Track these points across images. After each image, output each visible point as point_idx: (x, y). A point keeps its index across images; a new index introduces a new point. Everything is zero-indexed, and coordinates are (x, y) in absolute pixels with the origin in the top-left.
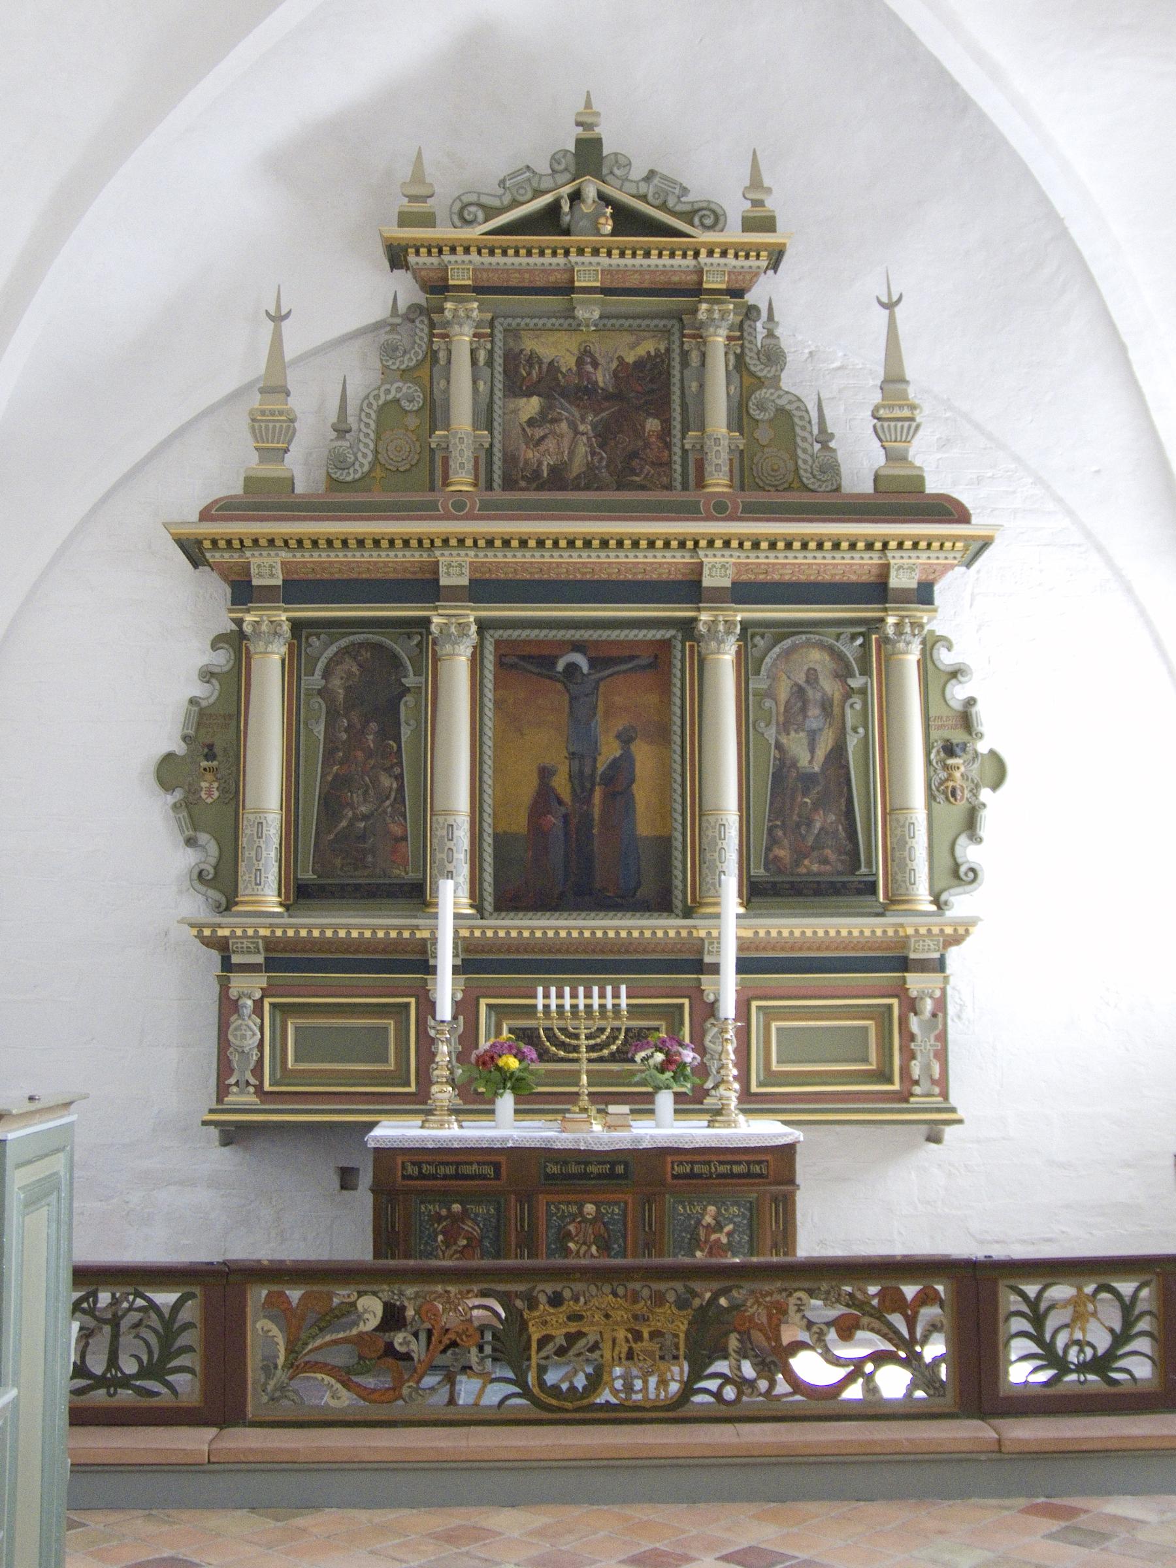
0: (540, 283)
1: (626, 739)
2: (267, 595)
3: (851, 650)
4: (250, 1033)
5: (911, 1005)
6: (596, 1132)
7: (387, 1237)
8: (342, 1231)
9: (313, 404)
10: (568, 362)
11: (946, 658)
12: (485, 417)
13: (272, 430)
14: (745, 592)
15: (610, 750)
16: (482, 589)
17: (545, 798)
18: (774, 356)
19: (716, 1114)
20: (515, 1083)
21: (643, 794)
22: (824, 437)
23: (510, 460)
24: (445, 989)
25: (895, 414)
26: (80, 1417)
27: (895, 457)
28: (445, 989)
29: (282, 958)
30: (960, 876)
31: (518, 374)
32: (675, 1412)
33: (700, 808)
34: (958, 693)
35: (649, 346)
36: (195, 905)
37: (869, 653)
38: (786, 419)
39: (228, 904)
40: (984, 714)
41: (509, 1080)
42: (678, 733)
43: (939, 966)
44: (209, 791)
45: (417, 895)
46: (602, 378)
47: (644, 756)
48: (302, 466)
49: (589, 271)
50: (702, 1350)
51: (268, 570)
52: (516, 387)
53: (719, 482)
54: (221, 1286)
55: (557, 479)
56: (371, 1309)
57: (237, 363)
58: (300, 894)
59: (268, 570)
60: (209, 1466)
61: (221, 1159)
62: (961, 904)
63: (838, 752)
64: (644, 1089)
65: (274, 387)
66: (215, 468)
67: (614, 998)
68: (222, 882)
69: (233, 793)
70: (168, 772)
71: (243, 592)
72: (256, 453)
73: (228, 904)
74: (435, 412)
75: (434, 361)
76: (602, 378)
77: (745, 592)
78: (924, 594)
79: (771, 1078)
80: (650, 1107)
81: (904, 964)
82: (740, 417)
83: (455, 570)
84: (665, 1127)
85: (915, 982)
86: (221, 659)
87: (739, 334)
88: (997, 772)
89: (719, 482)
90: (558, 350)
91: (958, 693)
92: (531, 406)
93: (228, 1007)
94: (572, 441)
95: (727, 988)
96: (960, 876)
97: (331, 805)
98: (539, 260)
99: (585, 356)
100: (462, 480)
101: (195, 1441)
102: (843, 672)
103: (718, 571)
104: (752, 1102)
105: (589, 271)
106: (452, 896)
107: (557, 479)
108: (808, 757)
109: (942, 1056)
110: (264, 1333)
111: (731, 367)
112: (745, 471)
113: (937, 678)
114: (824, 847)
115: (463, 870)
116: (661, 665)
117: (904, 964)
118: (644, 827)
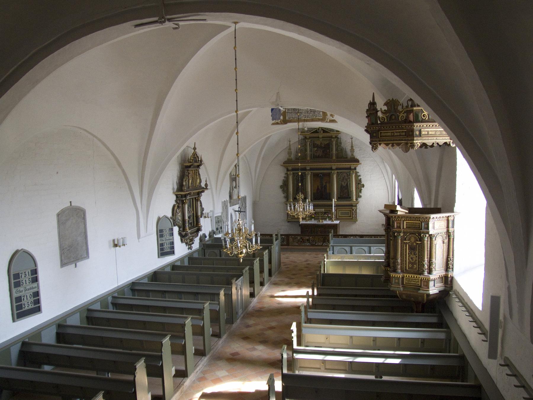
1: (326, 183)
2: (290, 170)
3: (348, 174)
5: (353, 210)
7: (302, 232)
8: (298, 231)
9: (293, 151)
10: (319, 144)
11: (358, 174)
12: (311, 151)
13: (290, 153)
14: (337, 169)
15: (324, 184)
16: (311, 169)
17: (318, 189)
18: (341, 143)
19: (332, 221)
20: (314, 218)
21: (328, 188)
22: (346, 151)
23: (314, 155)
25: (352, 150)
26: (281, 245)
27: (352, 155)
31: (315, 146)
32: (322, 246)
33: (333, 191)
34: (360, 178)
35: (328, 142)
37: (349, 176)
38: (342, 150)
40: (362, 180)
41: (313, 218)
42: (331, 182)
43: (356, 206)
44: (285, 189)
46: (323, 146)
47: (328, 185)
48: (293, 157)
49: (321, 136)
50: (324, 242)
51: (290, 168)
52: (314, 147)
53: (334, 158)
54: (287, 236)
55: (319, 157)
56: (299, 238)
57: (286, 145)
59: (290, 168)
60: (287, 249)
61: (287, 224)
63: (347, 184)
65: (290, 149)
66: (284, 157)
67: (323, 210)
69: (288, 189)
70: (281, 187)
71: (288, 170)
74: (306, 150)
75: (306, 145)
76: (323, 146)
77: (337, 169)
78: (355, 169)
79: (339, 217)
81: (352, 206)
82: (337, 150)
83: (308, 168)
84: (327, 222)
85: (353, 208)
86: (286, 175)
87: (337, 141)
88: (363, 186)
89: (334, 158)
90: (318, 143)
91: (360, 178)
92: (316, 149)
94: (320, 153)
98: (316, 135)
99: (321, 143)
100: (309, 158)
101: (286, 247)
102: (348, 176)
103: (334, 167)
104: (337, 219)
105: (321, 136)
107: (319, 157)
108: (344, 185)
109: (356, 215)
110: (291, 239)
112: (337, 157)
113: (357, 176)
114: (345, 194)
115: (310, 197)
116: (329, 175)
117: (352, 206)
118: (328, 192)
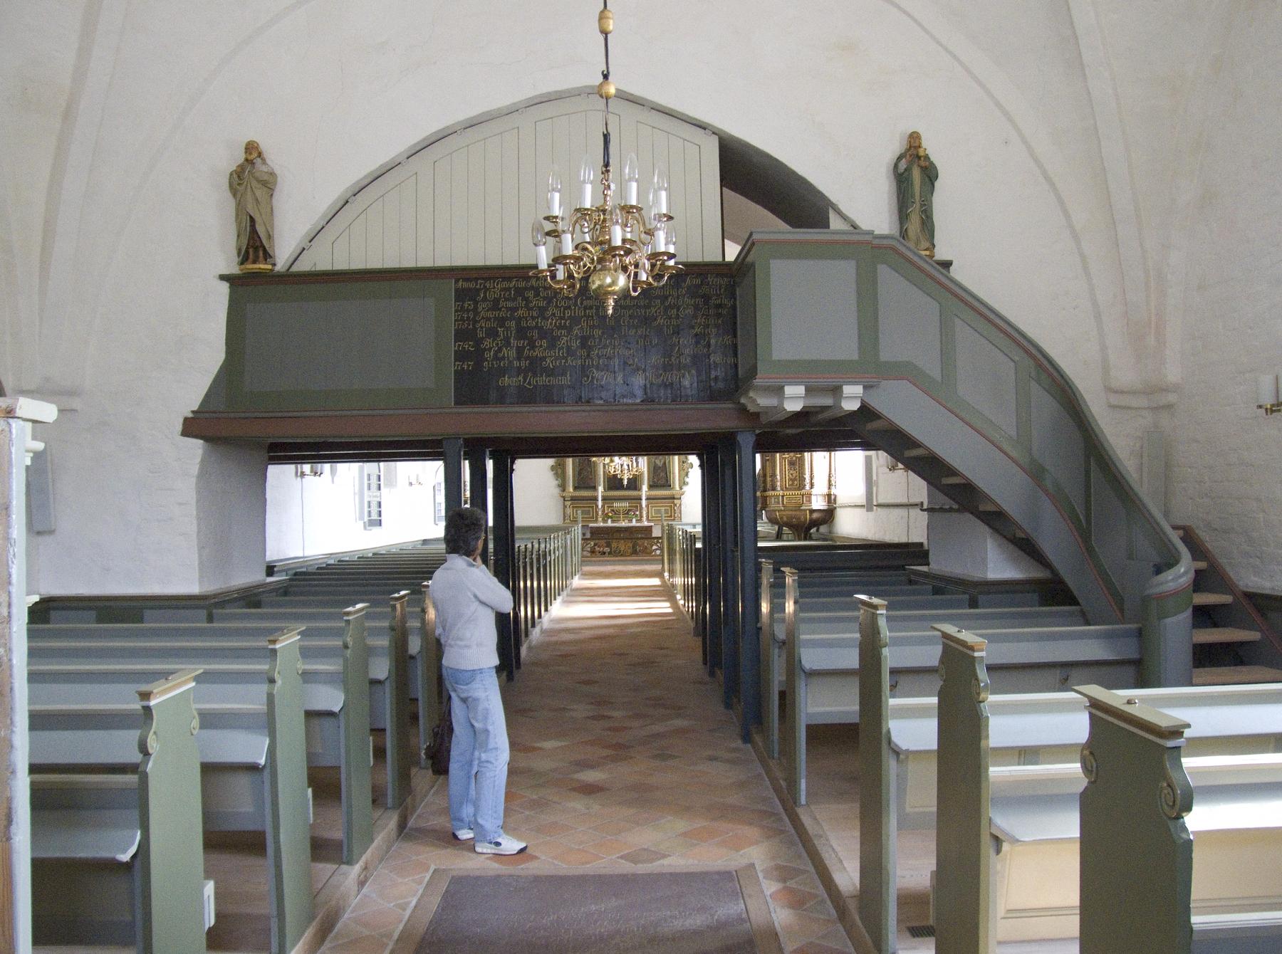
0: (366, 182)
4: (569, 511)
6: (624, 524)
24: (600, 503)
28: (600, 503)
29: (573, 499)
30: (685, 484)
36: (557, 491)
39: (564, 490)
45: (595, 488)
58: (575, 488)
62: (685, 488)
64: (373, 624)
67: (626, 504)
68: (563, 487)
72: (225, 287)
73: (564, 490)
80: (40, 777)
93: (565, 507)
95: (644, 503)
96: (685, 484)
97: (580, 474)
106: (601, 489)
111: (728, 472)
